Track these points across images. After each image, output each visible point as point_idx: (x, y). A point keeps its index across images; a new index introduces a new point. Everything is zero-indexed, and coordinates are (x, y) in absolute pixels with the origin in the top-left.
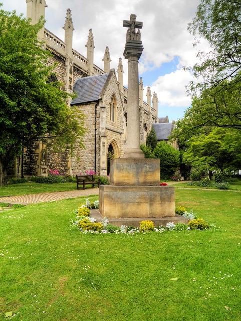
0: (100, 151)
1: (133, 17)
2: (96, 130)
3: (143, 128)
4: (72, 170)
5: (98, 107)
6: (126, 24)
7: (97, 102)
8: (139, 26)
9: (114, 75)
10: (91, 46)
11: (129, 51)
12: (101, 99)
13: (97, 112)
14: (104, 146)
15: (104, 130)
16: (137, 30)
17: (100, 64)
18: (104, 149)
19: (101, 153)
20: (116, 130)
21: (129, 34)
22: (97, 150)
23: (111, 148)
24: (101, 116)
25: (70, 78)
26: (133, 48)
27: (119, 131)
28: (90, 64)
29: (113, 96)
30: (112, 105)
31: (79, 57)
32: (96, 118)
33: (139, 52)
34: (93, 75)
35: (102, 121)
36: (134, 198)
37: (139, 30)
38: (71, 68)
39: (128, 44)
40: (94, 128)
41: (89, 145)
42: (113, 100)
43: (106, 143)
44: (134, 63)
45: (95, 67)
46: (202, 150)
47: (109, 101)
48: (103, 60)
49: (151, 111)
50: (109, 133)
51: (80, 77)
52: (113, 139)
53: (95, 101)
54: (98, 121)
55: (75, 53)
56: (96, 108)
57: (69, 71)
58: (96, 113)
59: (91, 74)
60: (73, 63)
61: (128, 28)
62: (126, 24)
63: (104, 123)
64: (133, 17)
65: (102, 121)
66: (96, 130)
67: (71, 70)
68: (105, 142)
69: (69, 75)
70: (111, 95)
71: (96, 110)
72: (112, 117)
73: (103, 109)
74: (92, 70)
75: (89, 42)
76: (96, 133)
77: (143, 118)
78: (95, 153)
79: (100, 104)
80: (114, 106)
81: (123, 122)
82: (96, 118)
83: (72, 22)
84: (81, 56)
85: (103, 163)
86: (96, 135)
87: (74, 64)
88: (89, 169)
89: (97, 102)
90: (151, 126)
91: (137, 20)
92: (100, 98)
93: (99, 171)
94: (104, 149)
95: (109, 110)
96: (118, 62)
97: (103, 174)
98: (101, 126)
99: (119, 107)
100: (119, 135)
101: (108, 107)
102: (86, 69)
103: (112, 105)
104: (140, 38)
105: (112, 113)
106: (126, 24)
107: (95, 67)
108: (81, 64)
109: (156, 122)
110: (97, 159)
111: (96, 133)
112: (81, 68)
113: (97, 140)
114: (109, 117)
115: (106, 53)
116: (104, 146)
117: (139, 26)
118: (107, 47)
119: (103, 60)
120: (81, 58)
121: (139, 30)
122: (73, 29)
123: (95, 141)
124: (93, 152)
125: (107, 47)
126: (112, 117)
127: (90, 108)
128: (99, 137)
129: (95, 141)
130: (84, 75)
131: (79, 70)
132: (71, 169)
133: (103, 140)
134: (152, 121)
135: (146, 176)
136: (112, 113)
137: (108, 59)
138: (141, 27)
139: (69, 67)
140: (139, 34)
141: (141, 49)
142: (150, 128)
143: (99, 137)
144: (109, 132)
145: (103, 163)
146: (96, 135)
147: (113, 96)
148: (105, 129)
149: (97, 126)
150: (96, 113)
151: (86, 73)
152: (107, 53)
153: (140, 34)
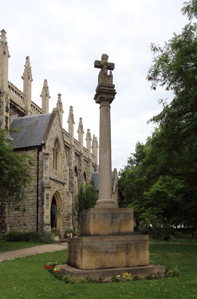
0: (43, 204)
1: (105, 57)
2: (38, 179)
3: (73, 171)
4: (10, 227)
5: (41, 154)
6: (97, 65)
7: (40, 148)
8: (111, 67)
9: (57, 116)
10: (29, 78)
11: (102, 96)
12: (44, 144)
13: (40, 159)
14: (47, 198)
15: (48, 180)
16: (109, 71)
17: (38, 102)
18: (48, 202)
19: (45, 206)
20: (59, 179)
21: (100, 77)
22: (40, 203)
23: (54, 201)
24: (44, 163)
25: (7, 118)
26: (110, 93)
27: (62, 181)
28: (27, 100)
29: (57, 140)
30: (56, 152)
31: (16, 92)
32: (38, 166)
33: (112, 97)
34: (32, 115)
35: (45, 169)
36: (111, 248)
37: (111, 72)
38: (7, 106)
39: (112, 97)
40: (36, 178)
41: (31, 198)
42: (57, 146)
43: (50, 195)
44: (106, 109)
45: (33, 104)
46: (148, 200)
47: (52, 146)
48: (41, 96)
49: (91, 158)
50: (52, 183)
51: (15, 117)
52: (56, 190)
53: (37, 146)
54: (40, 170)
55: (11, 86)
56: (38, 154)
57: (5, 109)
58: (38, 160)
59: (29, 113)
60: (9, 99)
61: (100, 70)
62: (98, 64)
63: (48, 171)
64: (105, 57)
65: (45, 169)
66: (38, 179)
67: (7, 108)
68: (49, 193)
69: (5, 114)
70: (54, 139)
71: (38, 157)
72: (55, 166)
73: (47, 156)
74: (30, 108)
75: (26, 74)
76: (38, 183)
77: (83, 165)
78: (38, 206)
79: (43, 150)
80: (57, 152)
81: (66, 171)
82: (38, 166)
83: (7, 48)
84: (17, 91)
85: (47, 218)
86: (38, 185)
87: (11, 100)
88: (34, 230)
89: (40, 148)
90: (91, 176)
91: (110, 61)
92: (43, 142)
93: (42, 228)
94: (48, 202)
95: (53, 156)
96: (57, 99)
97: (48, 229)
98: (44, 176)
99: (62, 153)
100: (61, 186)
101: (51, 153)
102: (23, 107)
103: (56, 152)
104: (112, 81)
105: (55, 160)
106: (97, 65)
107: (33, 104)
108: (18, 100)
109: (95, 170)
110: (39, 214)
111: (38, 183)
112: (18, 106)
113: (40, 192)
114: (52, 164)
115: (44, 87)
116: (47, 198)
117: (111, 67)
118: (46, 81)
119: (41, 96)
120: (17, 92)
121: (111, 72)
122: (9, 56)
123: (38, 193)
124: (35, 206)
125: (46, 81)
126: (55, 166)
127: (32, 154)
128: (42, 187)
129: (38, 193)
130: (22, 114)
131: (15, 107)
132: (8, 225)
133: (46, 191)
134: (92, 169)
135: (120, 226)
136: (55, 160)
137: (47, 95)
138: (112, 69)
139: (5, 104)
140: (111, 76)
141: (114, 93)
142: (89, 178)
143: (42, 187)
144: (52, 183)
145: (47, 218)
146: (38, 185)
147: (57, 140)
148: (48, 178)
149: (40, 175)
150: (38, 160)
151: (23, 111)
152: (46, 88)
153: (112, 77)
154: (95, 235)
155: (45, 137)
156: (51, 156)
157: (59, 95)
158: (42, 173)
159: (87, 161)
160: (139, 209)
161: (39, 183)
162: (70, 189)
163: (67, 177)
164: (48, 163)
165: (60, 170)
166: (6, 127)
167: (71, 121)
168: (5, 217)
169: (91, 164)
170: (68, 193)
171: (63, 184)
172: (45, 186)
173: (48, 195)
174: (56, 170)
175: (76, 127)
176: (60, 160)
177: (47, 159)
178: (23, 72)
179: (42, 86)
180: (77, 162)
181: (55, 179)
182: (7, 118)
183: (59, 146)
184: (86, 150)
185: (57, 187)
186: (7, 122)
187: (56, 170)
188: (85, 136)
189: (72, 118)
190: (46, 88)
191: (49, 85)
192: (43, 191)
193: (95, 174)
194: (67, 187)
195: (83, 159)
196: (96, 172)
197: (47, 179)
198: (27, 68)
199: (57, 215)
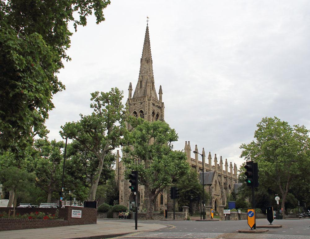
0: (212, 203)
7: (210, 185)
12: (212, 184)
14: (214, 201)
15: (214, 195)
19: (213, 204)
22: (211, 203)
23: (215, 202)
27: (218, 194)
30: (216, 185)
89: (210, 185)
90: (233, 186)
103: (216, 185)
109: (236, 182)
116: (214, 201)
118: (210, 152)
125: (210, 152)
133: (213, 199)
144: (215, 196)
147: (216, 181)
149: (211, 194)
155: (212, 181)
156: (214, 187)
157: (216, 154)
159: (231, 179)
160: (13, 173)
163: (220, 193)
164: (213, 190)
165: (217, 191)
167: (221, 163)
169: (233, 180)
170: (221, 199)
171: (219, 196)
173: (214, 200)
175: (224, 165)
176: (217, 188)
178: (150, 37)
180: (225, 181)
183: (217, 183)
184: (230, 174)
185: (216, 197)
188: (229, 167)
189: (222, 162)
191: (149, 28)
192: (212, 199)
193: (236, 185)
194: (220, 196)
195: (228, 179)
196: (236, 184)
199: (217, 207)
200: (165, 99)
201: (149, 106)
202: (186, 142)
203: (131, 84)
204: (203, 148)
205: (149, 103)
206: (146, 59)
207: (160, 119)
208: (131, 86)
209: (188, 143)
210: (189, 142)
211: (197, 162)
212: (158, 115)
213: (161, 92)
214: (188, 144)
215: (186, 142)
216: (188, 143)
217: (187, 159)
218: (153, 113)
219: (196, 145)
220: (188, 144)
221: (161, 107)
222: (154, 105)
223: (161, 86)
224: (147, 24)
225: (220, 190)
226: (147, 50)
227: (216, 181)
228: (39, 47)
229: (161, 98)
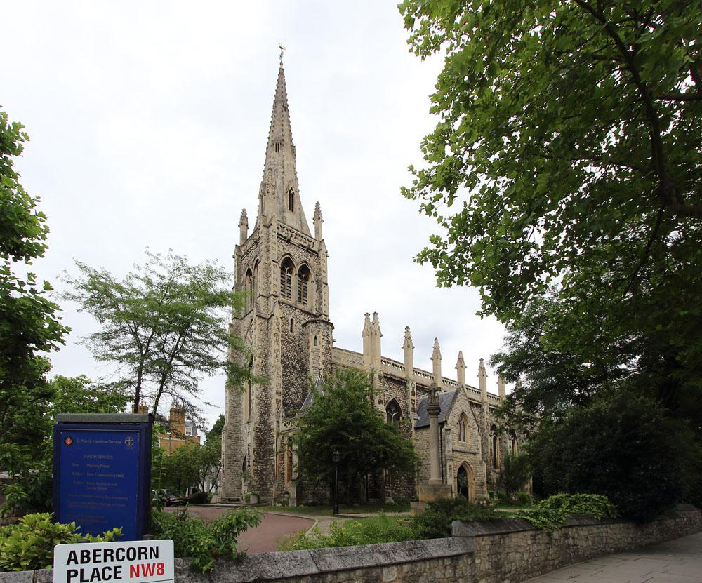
5: (443, 430)
12: (446, 421)
20: (467, 450)
22: (444, 473)
25: (413, 400)
27: (472, 451)
57: (411, 394)
69: (411, 397)
72: (462, 438)
79: (445, 427)
81: (478, 441)
92: (444, 420)
99: (471, 425)
105: (462, 433)
120: (425, 374)
125: (460, 352)
126: (462, 438)
133: (449, 463)
147: (463, 415)
149: (443, 448)
152: (461, 360)
154: (422, 501)
158: (445, 447)
161: (443, 456)
162: (482, 458)
163: (480, 447)
166: (413, 409)
168: (414, 485)
170: (481, 462)
171: (475, 454)
172: (447, 458)
174: (464, 441)
177: (449, 434)
179: (457, 358)
181: (462, 450)
182: (413, 400)
186: (413, 404)
187: (464, 441)
190: (461, 360)
191: (464, 356)
194: (479, 456)
197: (449, 451)
198: (435, 349)
200: (329, 235)
201: (268, 240)
202: (367, 315)
203: (244, 212)
204: (407, 328)
205: (268, 234)
206: (280, 143)
207: (314, 279)
208: (244, 217)
209: (372, 317)
210: (375, 314)
211: (408, 371)
212: (305, 271)
213: (318, 217)
214: (371, 321)
215: (367, 315)
216: (372, 317)
217: (481, 462)
218: (287, 264)
219: (407, 328)
220: (371, 321)
221: (315, 250)
222: (289, 241)
223: (318, 204)
224: (281, 64)
225: (479, 438)
226: (277, 122)
227: (463, 415)
228: (572, 564)
229: (318, 231)
